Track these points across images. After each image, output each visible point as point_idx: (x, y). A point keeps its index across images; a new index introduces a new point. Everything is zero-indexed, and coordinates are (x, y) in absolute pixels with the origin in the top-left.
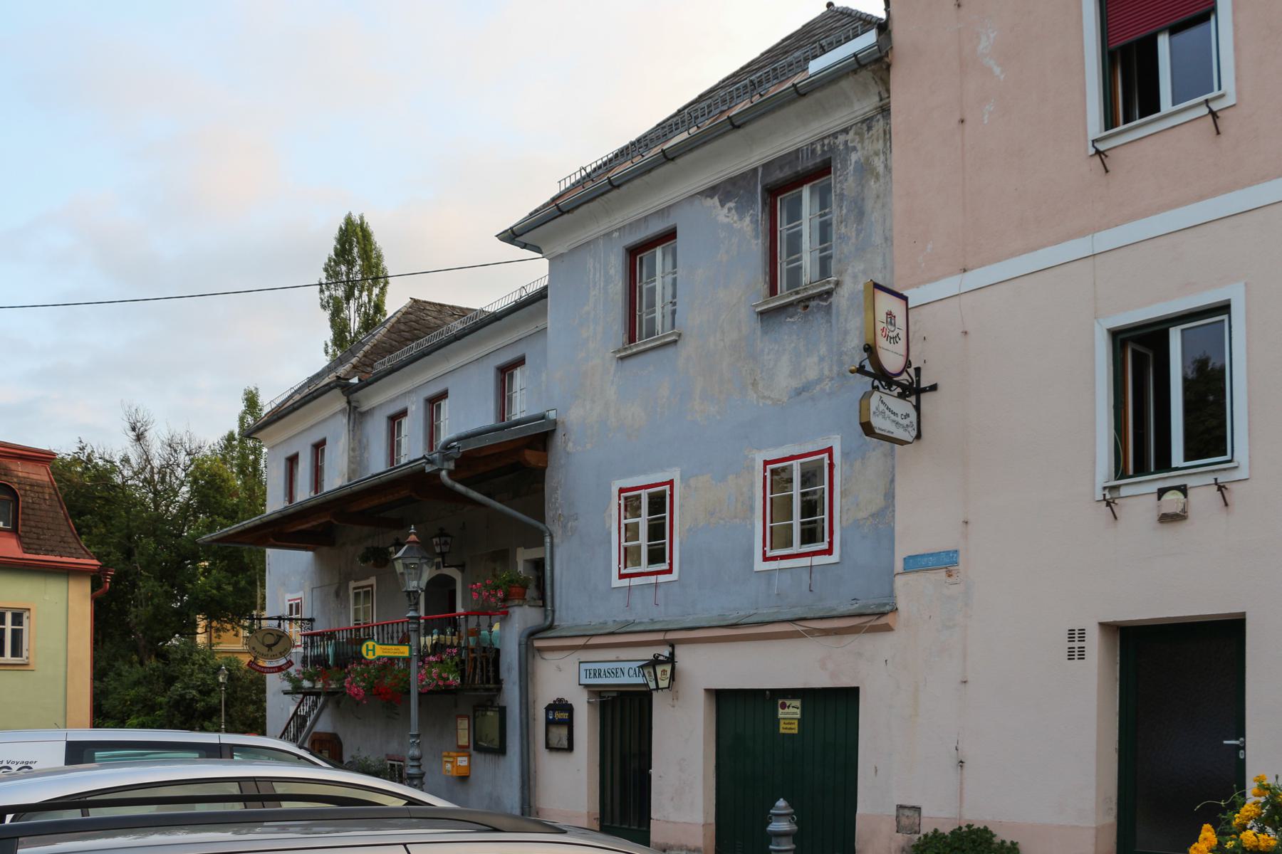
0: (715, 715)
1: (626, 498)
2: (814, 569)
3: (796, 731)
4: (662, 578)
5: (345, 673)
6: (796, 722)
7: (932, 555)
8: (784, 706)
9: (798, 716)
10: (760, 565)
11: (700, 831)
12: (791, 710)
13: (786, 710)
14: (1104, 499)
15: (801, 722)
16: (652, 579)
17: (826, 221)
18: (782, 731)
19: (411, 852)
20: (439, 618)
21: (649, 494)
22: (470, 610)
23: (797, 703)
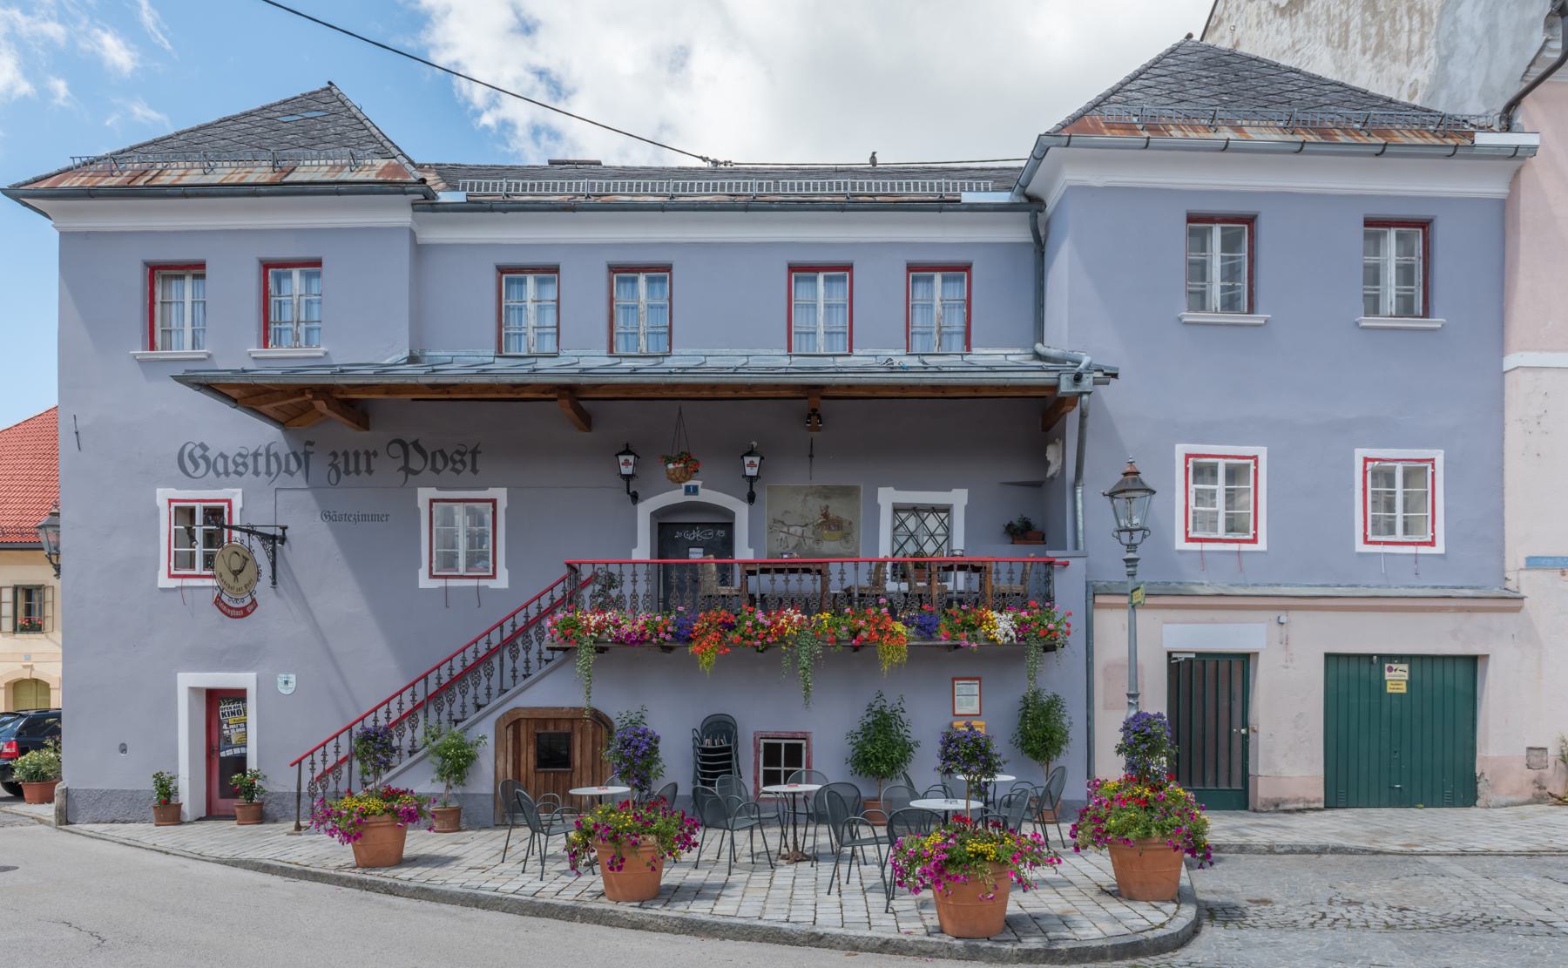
0: (1257, 682)
1: (176, 508)
2: (1420, 558)
3: (1404, 691)
4: (1245, 547)
5: (838, 613)
6: (1404, 683)
7: (1550, 558)
8: (1390, 669)
9: (1407, 678)
10: (1360, 547)
11: (490, 804)
12: (1398, 673)
13: (1393, 673)
14: (856, 562)
15: (1410, 683)
16: (1234, 547)
17: (1234, 295)
18: (1389, 691)
19: (1560, 843)
20: (677, 563)
21: (1227, 465)
22: (764, 558)
23: (1405, 667)
